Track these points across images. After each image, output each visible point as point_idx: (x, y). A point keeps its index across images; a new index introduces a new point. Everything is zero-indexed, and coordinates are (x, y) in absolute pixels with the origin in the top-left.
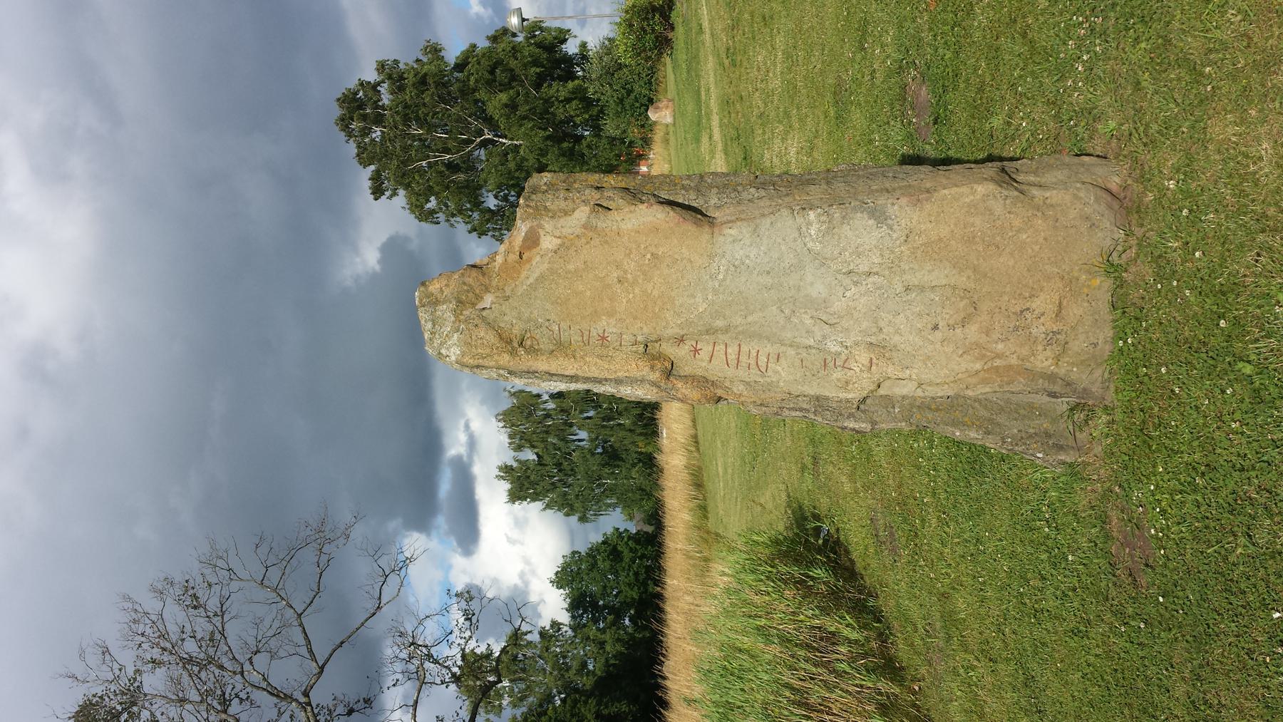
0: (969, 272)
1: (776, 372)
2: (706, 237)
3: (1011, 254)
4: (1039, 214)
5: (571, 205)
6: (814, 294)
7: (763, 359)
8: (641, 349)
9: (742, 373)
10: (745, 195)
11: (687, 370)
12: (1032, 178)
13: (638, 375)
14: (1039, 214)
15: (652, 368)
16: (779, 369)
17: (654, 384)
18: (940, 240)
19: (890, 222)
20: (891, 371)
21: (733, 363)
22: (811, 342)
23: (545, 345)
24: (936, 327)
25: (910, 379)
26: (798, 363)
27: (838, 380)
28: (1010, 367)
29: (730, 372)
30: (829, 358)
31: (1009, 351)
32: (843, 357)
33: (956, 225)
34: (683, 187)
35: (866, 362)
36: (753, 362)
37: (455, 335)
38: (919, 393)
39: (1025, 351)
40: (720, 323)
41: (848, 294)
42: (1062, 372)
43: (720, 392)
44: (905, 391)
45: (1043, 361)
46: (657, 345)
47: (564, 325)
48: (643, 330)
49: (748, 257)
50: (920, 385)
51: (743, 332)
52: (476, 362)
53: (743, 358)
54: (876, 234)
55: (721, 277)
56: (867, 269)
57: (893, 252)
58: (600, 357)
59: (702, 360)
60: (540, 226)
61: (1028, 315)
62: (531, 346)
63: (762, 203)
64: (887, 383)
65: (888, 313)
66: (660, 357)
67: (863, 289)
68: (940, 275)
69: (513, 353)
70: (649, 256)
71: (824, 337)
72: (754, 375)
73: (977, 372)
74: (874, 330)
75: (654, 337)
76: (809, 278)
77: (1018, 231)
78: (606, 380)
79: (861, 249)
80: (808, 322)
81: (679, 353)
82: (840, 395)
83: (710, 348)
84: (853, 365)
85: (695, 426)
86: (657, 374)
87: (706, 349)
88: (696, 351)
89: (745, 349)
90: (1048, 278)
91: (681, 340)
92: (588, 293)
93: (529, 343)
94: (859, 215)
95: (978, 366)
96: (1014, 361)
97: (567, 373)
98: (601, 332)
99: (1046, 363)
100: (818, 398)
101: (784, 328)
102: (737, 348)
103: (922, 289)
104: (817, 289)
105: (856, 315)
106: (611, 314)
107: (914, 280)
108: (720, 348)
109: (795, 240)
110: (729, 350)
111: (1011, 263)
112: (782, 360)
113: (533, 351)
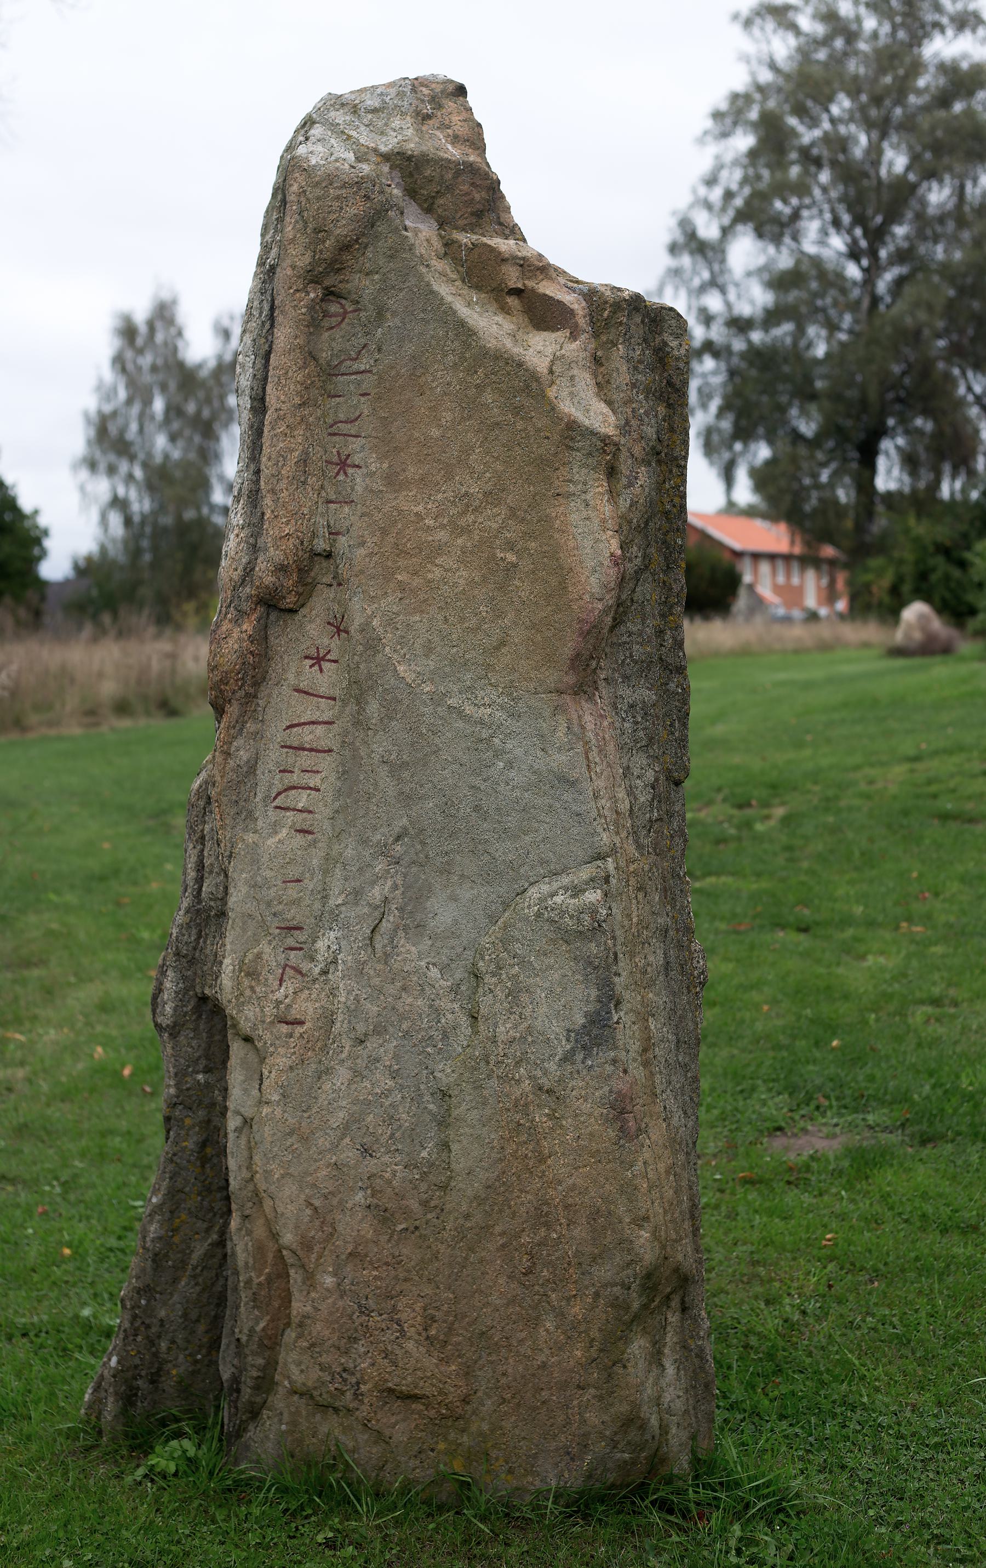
0: (478, 1218)
1: (275, 827)
2: (552, 677)
3: (512, 1301)
4: (594, 1352)
5: (617, 397)
6: (433, 903)
7: (303, 798)
8: (321, 545)
9: (273, 756)
10: (640, 760)
11: (278, 641)
12: (671, 1338)
13: (267, 539)
14: (594, 1352)
15: (281, 569)
16: (284, 832)
17: (249, 570)
18: (542, 1160)
19: (579, 1056)
20: (280, 1060)
21: (295, 736)
22: (336, 900)
23: (330, 344)
24: (366, 1151)
25: (261, 1102)
26: (293, 872)
27: (259, 956)
28: (287, 1300)
29: (276, 732)
30: (302, 936)
31: (317, 1300)
32: (305, 966)
33: (573, 1187)
34: (660, 632)
35: (294, 1014)
36: (295, 778)
37: (351, 156)
38: (233, 1123)
39: (318, 1329)
40: (373, 708)
41: (434, 972)
42: (278, 1400)
43: (233, 710)
44: (236, 1093)
45: (295, 1367)
46: (328, 579)
47: (369, 382)
48: (356, 552)
49: (510, 765)
50: (247, 1123)
51: (355, 757)
52: (291, 198)
53: (306, 760)
54: (556, 1029)
55: (469, 709)
56: (484, 1011)
57: (518, 1063)
58: (304, 461)
59: (299, 674)
60: (573, 337)
61: (390, 1336)
62: (326, 314)
63: (621, 794)
64: (252, 1057)
65: (396, 1057)
66: (306, 588)
67: (444, 1004)
68: (472, 1154)
69: (312, 277)
70: (511, 558)
71: (346, 926)
72: (268, 778)
73: (275, 1236)
74: (361, 1028)
75: (343, 570)
76: (466, 893)
77: (562, 1315)
78: (258, 472)
79: (524, 998)
80: (376, 893)
81: (312, 628)
82: (227, 961)
83: (323, 690)
84: (289, 987)
85: (311, 750)
86: (269, 580)
87: (326, 680)
88: (318, 660)
89: (326, 764)
90: (468, 1372)
91: (339, 627)
92: (435, 432)
93: (334, 308)
94: (594, 993)
95: (288, 1238)
96: (299, 1306)
97: (269, 388)
98: (356, 459)
99: (294, 1370)
100: (222, 914)
101: (364, 842)
102: (323, 744)
103: (443, 1122)
104: (443, 912)
105: (391, 989)
106: (393, 481)
107: (464, 1107)
108: (326, 711)
109: (543, 862)
110: (320, 730)
111: (495, 1299)
112: (300, 839)
113: (315, 322)
